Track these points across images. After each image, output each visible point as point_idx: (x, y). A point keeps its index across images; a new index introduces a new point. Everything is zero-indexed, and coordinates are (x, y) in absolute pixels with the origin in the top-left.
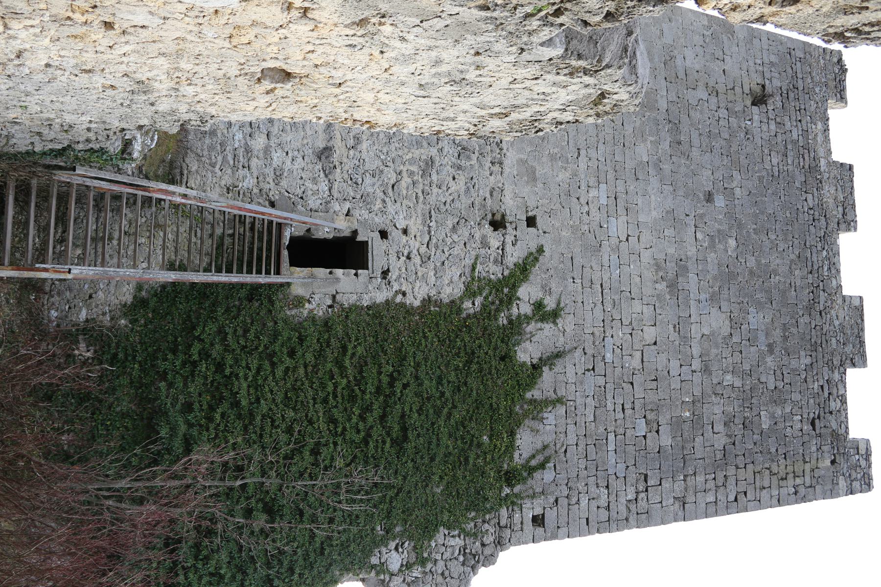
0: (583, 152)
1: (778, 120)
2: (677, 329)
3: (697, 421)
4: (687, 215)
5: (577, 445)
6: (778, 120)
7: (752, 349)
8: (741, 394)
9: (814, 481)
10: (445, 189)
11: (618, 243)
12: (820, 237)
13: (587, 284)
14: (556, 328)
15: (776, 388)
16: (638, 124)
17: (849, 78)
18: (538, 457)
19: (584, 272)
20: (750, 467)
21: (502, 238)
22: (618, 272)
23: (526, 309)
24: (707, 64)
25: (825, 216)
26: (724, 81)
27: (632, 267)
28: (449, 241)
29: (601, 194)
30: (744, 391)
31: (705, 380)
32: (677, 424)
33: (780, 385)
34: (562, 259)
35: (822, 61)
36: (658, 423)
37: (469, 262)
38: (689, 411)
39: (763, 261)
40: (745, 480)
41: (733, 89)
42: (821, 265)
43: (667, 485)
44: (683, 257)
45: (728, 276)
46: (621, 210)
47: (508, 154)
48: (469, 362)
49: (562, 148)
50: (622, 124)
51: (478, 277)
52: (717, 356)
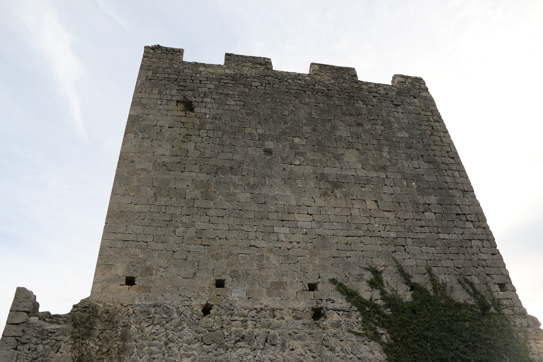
0: (253, 243)
1: (202, 95)
2: (363, 185)
3: (417, 178)
4: (284, 169)
5: (452, 260)
6: (202, 95)
7: (363, 137)
8: (392, 148)
9: (428, 110)
10: (302, 357)
11: (315, 222)
12: (280, 82)
13: (348, 247)
14: (384, 272)
15: (382, 125)
16: (222, 198)
17: (163, 44)
18: (467, 288)
19: (341, 248)
20: (433, 147)
21: (331, 311)
22: (336, 224)
23: (376, 294)
24: (166, 139)
25: (265, 76)
26: (178, 129)
27: (330, 213)
28: (342, 354)
29: (282, 232)
30: (390, 145)
31: (390, 170)
32: (422, 191)
33: (380, 122)
34: (336, 265)
35: (154, 60)
36: (424, 204)
37: (354, 338)
38: (411, 183)
39: (305, 121)
40: (440, 151)
41: (183, 123)
42: (298, 85)
43: (458, 201)
44: (315, 176)
45: (320, 147)
46: (291, 217)
47: (265, 304)
48: (425, 337)
49: (252, 259)
50: (224, 209)
51: (363, 330)
52: (373, 160)
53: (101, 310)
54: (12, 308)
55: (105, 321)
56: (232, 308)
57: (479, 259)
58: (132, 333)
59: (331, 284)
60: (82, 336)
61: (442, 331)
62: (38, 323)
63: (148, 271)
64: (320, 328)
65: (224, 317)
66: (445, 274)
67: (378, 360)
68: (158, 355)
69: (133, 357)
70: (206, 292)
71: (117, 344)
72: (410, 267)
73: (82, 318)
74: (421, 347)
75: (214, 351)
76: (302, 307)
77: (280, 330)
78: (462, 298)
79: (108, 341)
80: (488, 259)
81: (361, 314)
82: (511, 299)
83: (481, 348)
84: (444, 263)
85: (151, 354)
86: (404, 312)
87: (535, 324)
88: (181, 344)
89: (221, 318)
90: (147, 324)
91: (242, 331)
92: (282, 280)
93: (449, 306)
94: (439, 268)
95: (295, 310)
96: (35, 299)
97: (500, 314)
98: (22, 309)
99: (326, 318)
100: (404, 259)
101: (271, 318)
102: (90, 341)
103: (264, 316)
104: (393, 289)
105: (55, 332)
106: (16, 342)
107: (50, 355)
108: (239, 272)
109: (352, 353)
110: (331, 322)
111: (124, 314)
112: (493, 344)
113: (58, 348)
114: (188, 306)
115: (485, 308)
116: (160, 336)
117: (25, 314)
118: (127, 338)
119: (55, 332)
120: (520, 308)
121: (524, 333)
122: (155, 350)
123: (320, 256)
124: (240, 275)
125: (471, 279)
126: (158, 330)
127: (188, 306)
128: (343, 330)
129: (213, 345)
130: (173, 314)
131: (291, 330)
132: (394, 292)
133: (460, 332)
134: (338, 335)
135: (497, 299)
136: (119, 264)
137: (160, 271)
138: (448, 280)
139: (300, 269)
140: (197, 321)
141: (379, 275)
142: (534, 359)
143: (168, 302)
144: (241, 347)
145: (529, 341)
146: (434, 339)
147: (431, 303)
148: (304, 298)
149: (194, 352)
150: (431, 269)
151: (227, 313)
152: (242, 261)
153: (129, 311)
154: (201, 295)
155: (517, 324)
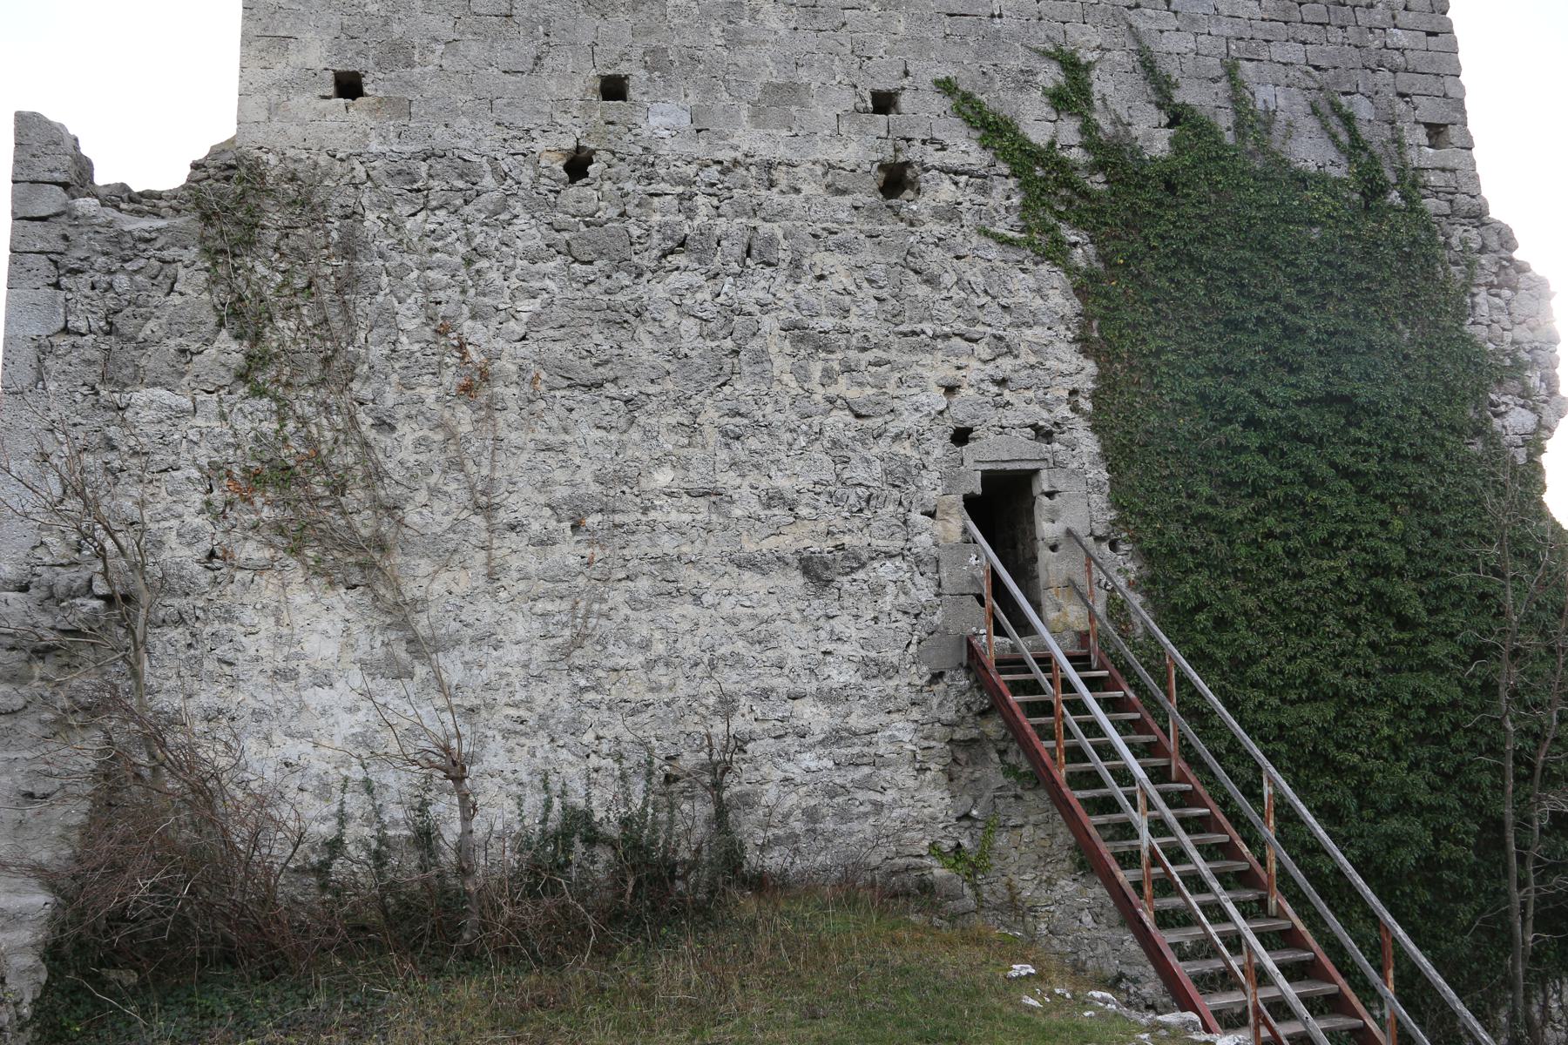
5: (1304, 43)
10: (848, 298)
14: (1098, 66)
21: (934, 172)
23: (1069, 131)
34: (957, 39)
37: (994, 252)
47: (745, 148)
48: (1192, 260)
53: (273, 173)
54: (15, 174)
55: (289, 204)
56: (651, 159)
57: (1385, 46)
58: (371, 234)
59: (941, 96)
60: (231, 247)
61: (1243, 248)
62: (102, 214)
63: (398, 54)
64: (902, 220)
65: (629, 186)
66: (1277, 85)
67: (1056, 313)
68: (449, 292)
69: (380, 298)
70: (575, 114)
71: (330, 268)
72: (1175, 56)
73: (222, 196)
74: (1179, 285)
75: (603, 280)
76: (853, 160)
77: (789, 224)
78: (1313, 157)
79: (304, 258)
80: (1412, 46)
81: (1021, 185)
82: (1453, 171)
83: (1342, 299)
84: (1277, 51)
85: (428, 289)
86: (1142, 187)
87: (1502, 245)
88: (510, 262)
89: (619, 189)
90: (408, 209)
91: (680, 223)
92: (796, 80)
93: (1273, 179)
94: (1261, 64)
95: (831, 166)
96: (76, 148)
97: (1412, 210)
98: (47, 176)
99: (918, 191)
100: (1161, 32)
101: (762, 188)
102: (254, 259)
103: (742, 182)
104: (1119, 118)
105: (155, 239)
106: (52, 268)
107: (154, 301)
108: (670, 52)
109: (986, 292)
110: (934, 204)
111: (343, 181)
112: (1375, 291)
113: (169, 281)
114: (524, 155)
115: (1373, 189)
116: (449, 240)
117: (59, 189)
118: (358, 248)
119: (155, 239)
120: (1473, 197)
121: (1467, 266)
122: (440, 281)
123: (912, 10)
124: (671, 62)
125: (1351, 104)
126: (441, 224)
127: (524, 155)
128: (965, 229)
129: (599, 264)
130: (481, 177)
131: (819, 225)
132: (1120, 127)
133: (1292, 253)
134: (951, 241)
135: (1415, 169)
136: (309, 35)
137: (433, 52)
138: (1281, 102)
139: (850, 46)
140: (551, 197)
141: (1083, 75)
142: (1474, 336)
143: (464, 143)
144: (677, 269)
145: (1475, 290)
146: (1218, 268)
147: (1224, 167)
148: (860, 132)
149: (547, 282)
150: (1236, 67)
151: (637, 174)
152: (676, 21)
153: (355, 173)
154: (560, 121)
155: (1454, 241)
